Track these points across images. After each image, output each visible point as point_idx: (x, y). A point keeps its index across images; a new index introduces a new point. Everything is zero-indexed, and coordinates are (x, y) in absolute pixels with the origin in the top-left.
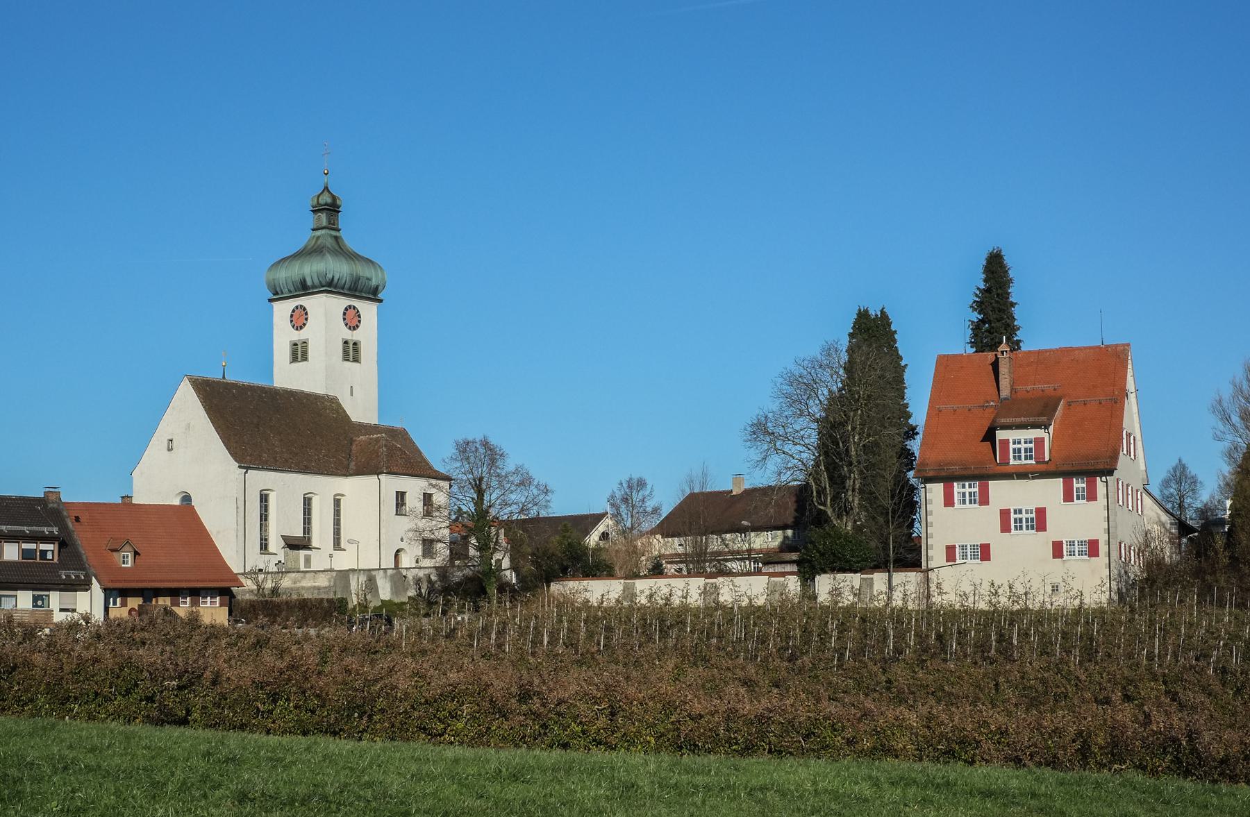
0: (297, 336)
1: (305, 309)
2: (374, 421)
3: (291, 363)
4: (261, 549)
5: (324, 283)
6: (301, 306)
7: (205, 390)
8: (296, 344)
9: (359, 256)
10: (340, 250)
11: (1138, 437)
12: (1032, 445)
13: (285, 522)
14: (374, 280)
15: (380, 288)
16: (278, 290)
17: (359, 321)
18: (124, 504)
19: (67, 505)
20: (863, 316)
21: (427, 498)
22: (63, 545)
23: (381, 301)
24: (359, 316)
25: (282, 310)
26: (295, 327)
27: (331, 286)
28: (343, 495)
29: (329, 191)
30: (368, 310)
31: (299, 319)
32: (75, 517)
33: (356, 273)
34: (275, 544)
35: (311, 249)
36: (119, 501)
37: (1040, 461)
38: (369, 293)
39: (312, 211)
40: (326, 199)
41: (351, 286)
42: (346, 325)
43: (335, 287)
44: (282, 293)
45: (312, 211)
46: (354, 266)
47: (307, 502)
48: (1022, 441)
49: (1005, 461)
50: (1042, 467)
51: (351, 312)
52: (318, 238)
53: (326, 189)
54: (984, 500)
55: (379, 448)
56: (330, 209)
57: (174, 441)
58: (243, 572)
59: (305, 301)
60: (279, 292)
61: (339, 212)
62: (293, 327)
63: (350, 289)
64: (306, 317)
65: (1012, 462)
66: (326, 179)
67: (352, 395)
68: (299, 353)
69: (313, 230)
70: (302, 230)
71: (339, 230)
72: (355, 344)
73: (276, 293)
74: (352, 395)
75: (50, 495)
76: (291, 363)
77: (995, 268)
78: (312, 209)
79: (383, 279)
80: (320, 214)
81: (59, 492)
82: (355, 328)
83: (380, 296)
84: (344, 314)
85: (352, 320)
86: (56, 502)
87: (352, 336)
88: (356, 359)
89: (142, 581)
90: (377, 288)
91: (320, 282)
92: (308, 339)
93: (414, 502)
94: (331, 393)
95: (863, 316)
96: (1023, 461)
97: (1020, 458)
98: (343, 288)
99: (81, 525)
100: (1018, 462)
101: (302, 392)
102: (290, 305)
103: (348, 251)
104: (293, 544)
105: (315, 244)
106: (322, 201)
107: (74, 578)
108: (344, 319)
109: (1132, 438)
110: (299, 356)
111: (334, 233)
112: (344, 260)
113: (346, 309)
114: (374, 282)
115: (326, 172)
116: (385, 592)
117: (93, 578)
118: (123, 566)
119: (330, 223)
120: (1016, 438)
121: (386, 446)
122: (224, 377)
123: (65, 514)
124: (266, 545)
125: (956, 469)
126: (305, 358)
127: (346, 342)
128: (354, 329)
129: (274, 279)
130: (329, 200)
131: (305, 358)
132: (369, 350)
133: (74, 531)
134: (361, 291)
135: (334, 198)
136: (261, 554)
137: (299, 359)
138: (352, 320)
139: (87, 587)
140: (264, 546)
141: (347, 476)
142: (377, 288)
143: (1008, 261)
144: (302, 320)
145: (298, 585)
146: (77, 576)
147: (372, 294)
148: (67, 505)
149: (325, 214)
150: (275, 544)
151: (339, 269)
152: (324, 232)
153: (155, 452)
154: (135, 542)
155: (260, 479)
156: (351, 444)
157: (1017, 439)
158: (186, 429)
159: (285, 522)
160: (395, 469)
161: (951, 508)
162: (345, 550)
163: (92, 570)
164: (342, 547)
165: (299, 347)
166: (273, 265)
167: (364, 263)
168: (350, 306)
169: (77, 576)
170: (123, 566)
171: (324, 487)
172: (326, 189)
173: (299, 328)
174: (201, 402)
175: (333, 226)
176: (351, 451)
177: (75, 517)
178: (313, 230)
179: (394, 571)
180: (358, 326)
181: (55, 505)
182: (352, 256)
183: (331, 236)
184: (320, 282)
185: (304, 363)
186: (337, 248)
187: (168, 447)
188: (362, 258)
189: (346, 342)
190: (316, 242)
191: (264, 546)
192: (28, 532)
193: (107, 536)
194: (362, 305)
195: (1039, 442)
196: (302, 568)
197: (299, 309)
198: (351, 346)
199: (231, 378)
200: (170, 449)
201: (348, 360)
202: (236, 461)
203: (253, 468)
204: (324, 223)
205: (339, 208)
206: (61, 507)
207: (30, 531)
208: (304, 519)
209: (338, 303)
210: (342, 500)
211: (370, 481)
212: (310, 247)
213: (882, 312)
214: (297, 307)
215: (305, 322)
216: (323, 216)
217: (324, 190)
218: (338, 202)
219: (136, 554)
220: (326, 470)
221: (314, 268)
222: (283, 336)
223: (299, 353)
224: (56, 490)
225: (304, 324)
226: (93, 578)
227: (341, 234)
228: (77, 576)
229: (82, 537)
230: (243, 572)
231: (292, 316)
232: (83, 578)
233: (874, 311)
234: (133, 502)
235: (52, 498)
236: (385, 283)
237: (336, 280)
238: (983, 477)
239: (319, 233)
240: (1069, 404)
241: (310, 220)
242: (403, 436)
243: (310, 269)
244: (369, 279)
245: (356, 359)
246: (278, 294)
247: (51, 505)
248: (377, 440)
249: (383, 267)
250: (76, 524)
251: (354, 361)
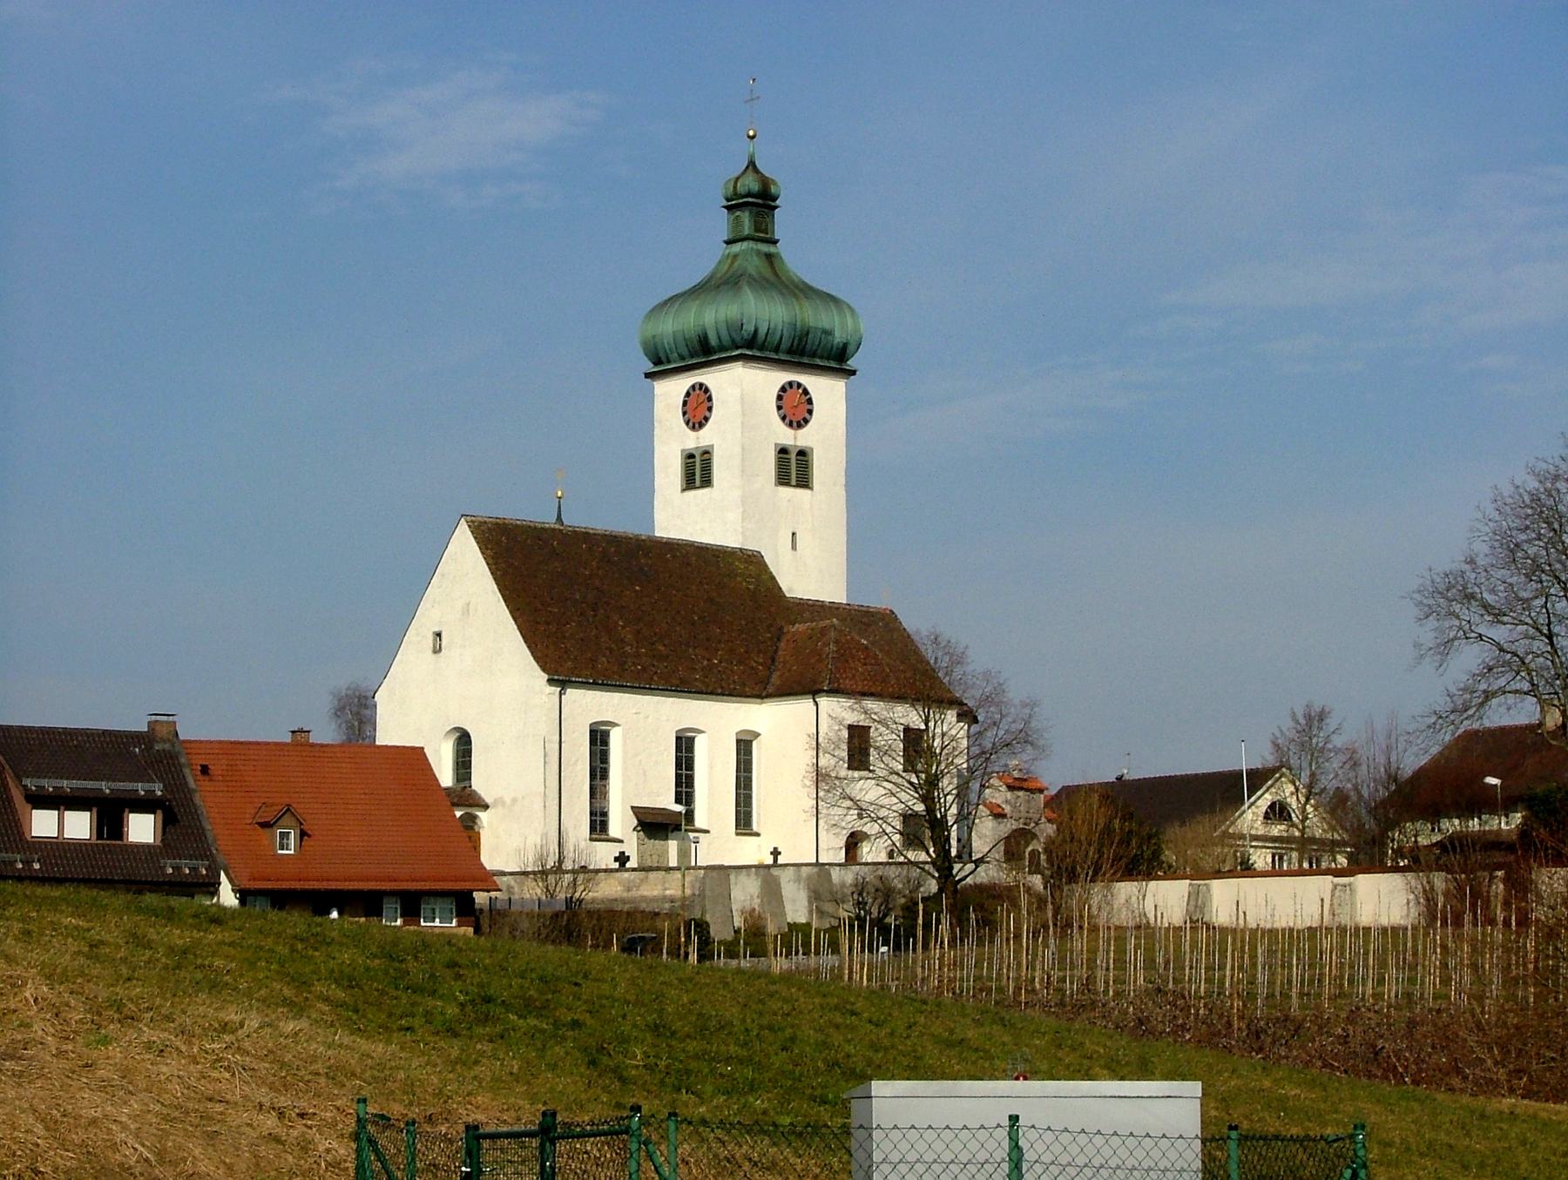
0: (693, 440)
1: (707, 390)
3: (683, 490)
5: (738, 339)
6: (701, 385)
7: (499, 543)
8: (691, 456)
9: (811, 288)
10: (775, 279)
14: (837, 334)
15: (851, 348)
16: (662, 355)
17: (810, 412)
18: (295, 744)
19: (188, 745)
21: (914, 742)
22: (169, 822)
23: (853, 373)
24: (810, 401)
25: (671, 391)
26: (691, 424)
29: (756, 170)
30: (827, 392)
31: (698, 409)
32: (201, 766)
33: (803, 320)
34: (620, 822)
35: (721, 278)
36: (288, 739)
38: (828, 359)
39: (725, 207)
40: (751, 183)
41: (792, 345)
42: (783, 418)
43: (762, 348)
44: (669, 362)
45: (725, 207)
46: (797, 308)
47: (685, 746)
51: (794, 396)
52: (735, 256)
53: (752, 165)
55: (825, 645)
57: (444, 635)
58: (814, 861)
59: (713, 378)
60: (664, 359)
61: (776, 207)
62: (687, 423)
63: (790, 352)
64: (709, 404)
66: (751, 147)
67: (794, 547)
68: (697, 471)
69: (728, 242)
71: (775, 242)
73: (657, 362)
74: (794, 547)
75: (157, 728)
76: (683, 490)
78: (725, 203)
79: (857, 330)
80: (738, 213)
81: (175, 723)
82: (799, 423)
83: (852, 363)
84: (780, 398)
85: (796, 409)
86: (169, 740)
87: (795, 438)
88: (804, 482)
90: (845, 346)
91: (733, 341)
92: (713, 446)
93: (887, 739)
94: (751, 546)
98: (777, 350)
99: (210, 780)
103: (793, 282)
104: (654, 825)
105: (727, 271)
106: (741, 189)
107: (187, 871)
108: (779, 408)
110: (698, 477)
111: (764, 248)
113: (783, 389)
114: (839, 338)
115: (751, 133)
116: (797, 909)
117: (222, 873)
118: (280, 852)
119: (757, 230)
121: (837, 642)
123: (183, 760)
126: (707, 482)
128: (799, 426)
129: (654, 337)
130: (755, 186)
131: (707, 482)
132: (828, 466)
133: (196, 791)
134: (813, 355)
135: (765, 182)
136: (591, 840)
137: (698, 483)
138: (796, 409)
139: (212, 889)
140: (599, 824)
141: (762, 698)
144: (703, 412)
145: (634, 893)
146: (194, 868)
148: (188, 745)
149: (747, 214)
150: (620, 822)
152: (745, 245)
153: (412, 656)
154: (301, 811)
155: (588, 705)
156: (779, 639)
158: (463, 614)
160: (847, 684)
161: (426, 750)
162: (758, 835)
163: (221, 859)
164: (755, 828)
165: (698, 459)
166: (653, 310)
167: (818, 302)
168: (790, 384)
170: (280, 852)
172: (752, 165)
173: (697, 426)
174: (488, 564)
175: (763, 234)
176: (776, 652)
177: (201, 766)
178: (728, 242)
179: (816, 870)
180: (806, 421)
181: (167, 746)
182: (801, 291)
183: (759, 252)
184: (733, 341)
187: (434, 646)
190: (732, 263)
191: (599, 824)
192: (108, 791)
193: (256, 800)
196: (673, 863)
197: (698, 391)
198: (793, 456)
199: (577, 519)
200: (437, 650)
202: (544, 670)
204: (747, 228)
206: (177, 748)
207: (112, 790)
208: (678, 776)
209: (762, 382)
210: (696, 739)
211: (800, 709)
212: (719, 275)
214: (693, 387)
215: (707, 414)
217: (747, 168)
218: (773, 190)
219: (303, 834)
220: (722, 687)
223: (697, 471)
224: (171, 718)
225: (706, 419)
226: (222, 873)
227: (781, 249)
228: (194, 869)
229: (209, 801)
230: (814, 861)
231: (685, 403)
232: (204, 872)
234: (378, 743)
235: (162, 732)
236: (861, 338)
239: (737, 248)
241: (721, 224)
242: (887, 625)
243: (712, 316)
245: (804, 482)
246: (663, 363)
247: (157, 747)
249: (857, 310)
250: (201, 777)
251: (798, 486)
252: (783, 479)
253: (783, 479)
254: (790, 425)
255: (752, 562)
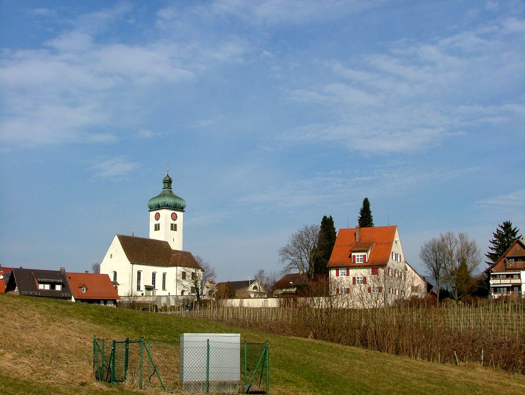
0: (157, 222)
1: (159, 214)
2: (182, 250)
4: (137, 289)
8: (156, 225)
10: (171, 195)
11: (402, 256)
12: (362, 257)
13: (146, 281)
15: (184, 207)
17: (177, 218)
20: (325, 217)
22: (63, 286)
23: (184, 211)
24: (177, 216)
25: (153, 214)
27: (167, 207)
28: (142, 271)
30: (180, 214)
31: (157, 217)
34: (143, 288)
36: (85, 272)
37: (365, 262)
47: (154, 275)
48: (360, 256)
49: (354, 262)
50: (365, 264)
52: (164, 191)
54: (348, 274)
56: (168, 182)
59: (159, 211)
65: (356, 262)
68: (157, 228)
69: (164, 189)
70: (160, 188)
71: (171, 189)
72: (175, 225)
77: (366, 203)
83: (184, 210)
84: (172, 215)
85: (174, 217)
88: (176, 230)
89: (92, 297)
90: (183, 207)
93: (189, 274)
95: (325, 217)
96: (360, 262)
97: (359, 261)
98: (171, 207)
100: (358, 262)
101: (156, 240)
102: (155, 212)
104: (148, 288)
108: (171, 217)
109: (399, 256)
111: (170, 190)
112: (172, 199)
113: (172, 214)
114: (182, 205)
116: (173, 303)
119: (168, 187)
120: (358, 255)
122: (133, 235)
124: (140, 289)
125: (339, 265)
126: (159, 229)
127: (172, 224)
128: (175, 220)
130: (168, 179)
131: (159, 229)
132: (180, 227)
135: (170, 179)
138: (174, 217)
140: (139, 288)
142: (183, 207)
143: (369, 200)
144: (158, 217)
147: (181, 209)
150: (143, 288)
151: (170, 201)
155: (137, 267)
157: (358, 256)
159: (146, 281)
165: (157, 226)
168: (174, 213)
169: (67, 295)
171: (160, 271)
172: (168, 175)
178: (164, 189)
182: (176, 197)
185: (159, 231)
186: (170, 194)
188: (178, 197)
189: (172, 224)
191: (139, 288)
194: (178, 213)
195: (365, 256)
196: (151, 295)
200: (111, 258)
201: (173, 230)
203: (135, 264)
205: (172, 181)
209: (169, 212)
211: (174, 268)
213: (331, 217)
216: (166, 184)
219: (87, 289)
221: (162, 201)
222: (153, 222)
229: (70, 283)
233: (328, 217)
235: (62, 271)
237: (169, 205)
238: (348, 268)
239: (165, 189)
240: (376, 244)
243: (160, 201)
244: (180, 204)
245: (176, 230)
246: (152, 209)
247: (62, 273)
248: (178, 255)
252: (172, 229)
253: (172, 229)
254: (173, 220)
255: (166, 243)
